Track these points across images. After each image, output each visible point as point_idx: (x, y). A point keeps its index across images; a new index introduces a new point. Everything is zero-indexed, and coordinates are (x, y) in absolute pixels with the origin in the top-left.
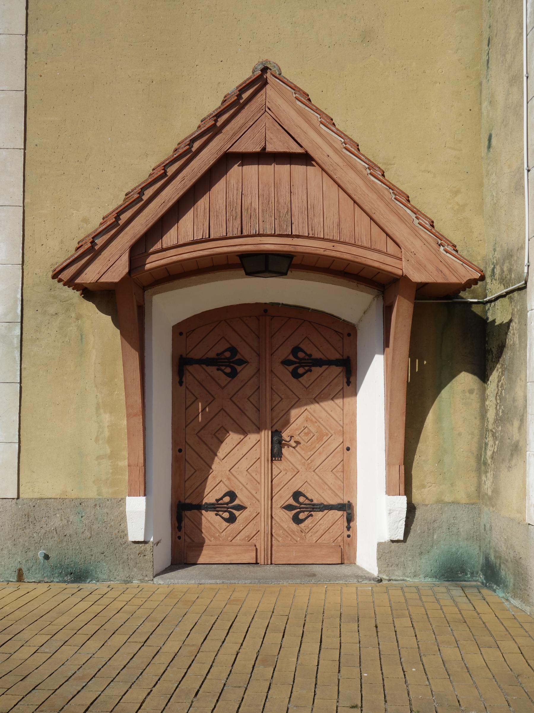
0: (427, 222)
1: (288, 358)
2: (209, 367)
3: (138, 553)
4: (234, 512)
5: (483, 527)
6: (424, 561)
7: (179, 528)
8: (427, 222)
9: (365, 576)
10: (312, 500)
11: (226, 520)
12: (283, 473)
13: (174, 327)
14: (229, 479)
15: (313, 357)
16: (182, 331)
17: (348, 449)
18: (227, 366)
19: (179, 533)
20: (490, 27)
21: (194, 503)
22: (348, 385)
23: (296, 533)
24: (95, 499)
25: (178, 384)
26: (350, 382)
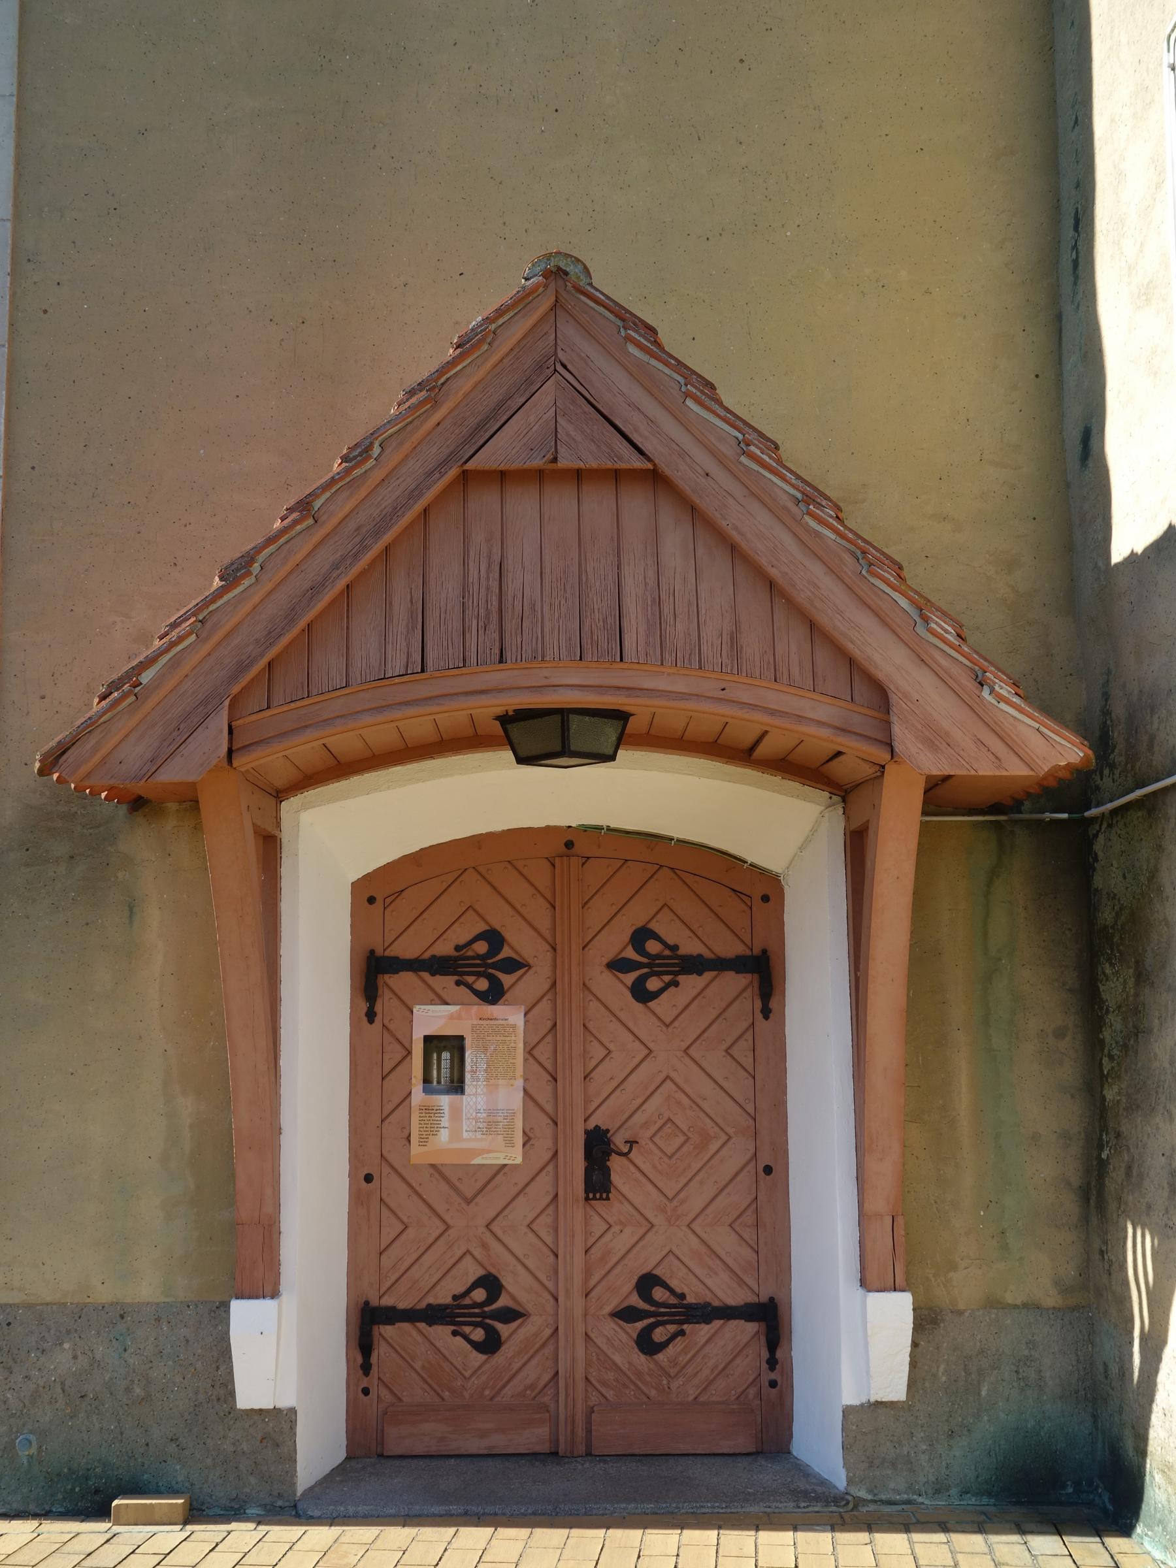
0: (950, 629)
1: (623, 955)
2: (438, 977)
3: (259, 1438)
4: (499, 1326)
5: (1101, 1368)
6: (957, 1454)
7: (366, 1368)
8: (950, 629)
9: (814, 1491)
10: (682, 1296)
11: (478, 1347)
12: (616, 1228)
13: (356, 886)
14: (485, 1246)
15: (682, 951)
16: (374, 894)
17: (768, 1170)
18: (479, 975)
19: (366, 1379)
20: (1078, 186)
21: (402, 1306)
22: (766, 1017)
23: (648, 1378)
24: (158, 1304)
25: (365, 1019)
26: (770, 1011)
